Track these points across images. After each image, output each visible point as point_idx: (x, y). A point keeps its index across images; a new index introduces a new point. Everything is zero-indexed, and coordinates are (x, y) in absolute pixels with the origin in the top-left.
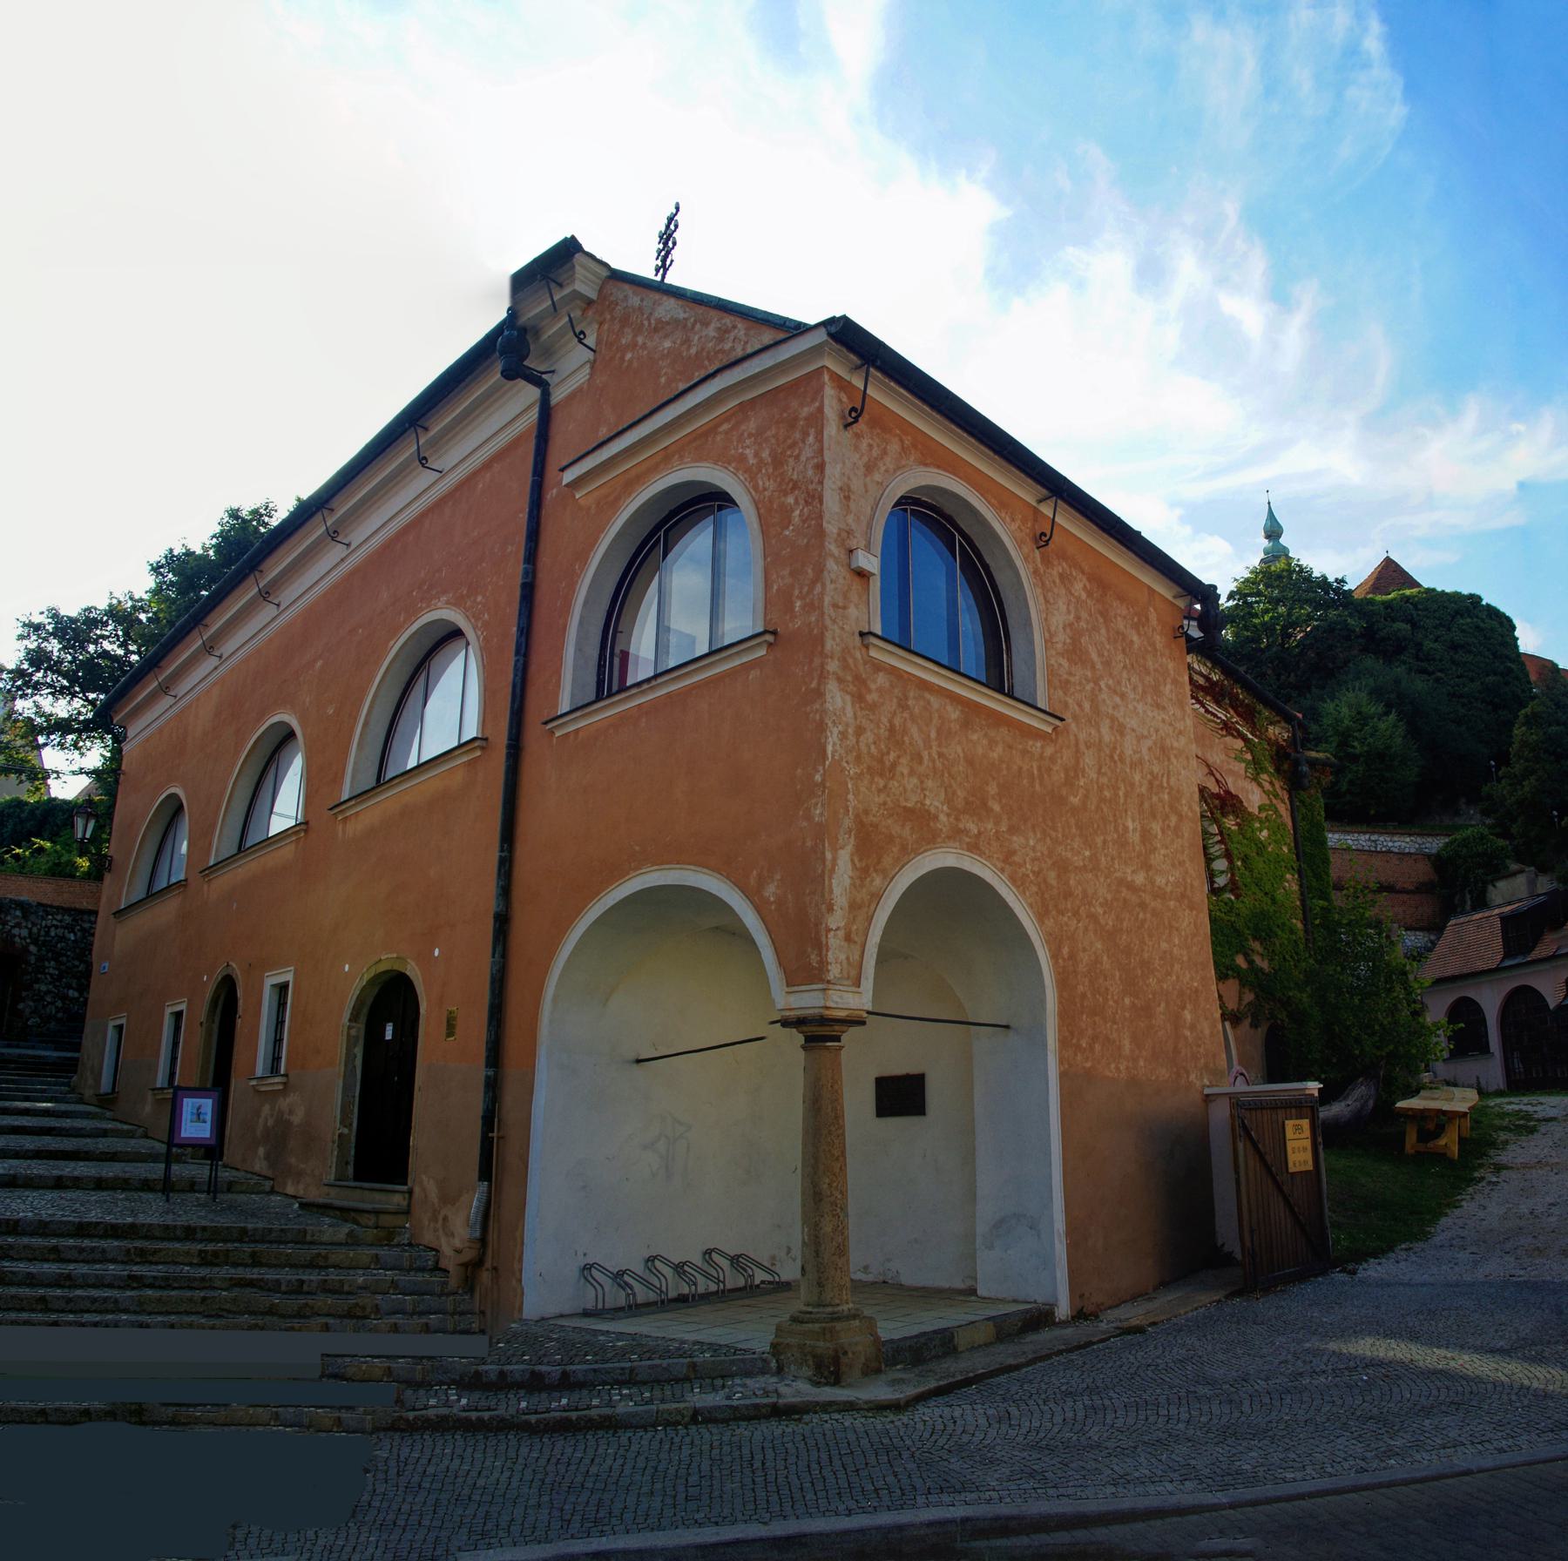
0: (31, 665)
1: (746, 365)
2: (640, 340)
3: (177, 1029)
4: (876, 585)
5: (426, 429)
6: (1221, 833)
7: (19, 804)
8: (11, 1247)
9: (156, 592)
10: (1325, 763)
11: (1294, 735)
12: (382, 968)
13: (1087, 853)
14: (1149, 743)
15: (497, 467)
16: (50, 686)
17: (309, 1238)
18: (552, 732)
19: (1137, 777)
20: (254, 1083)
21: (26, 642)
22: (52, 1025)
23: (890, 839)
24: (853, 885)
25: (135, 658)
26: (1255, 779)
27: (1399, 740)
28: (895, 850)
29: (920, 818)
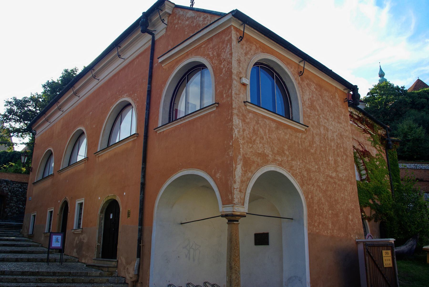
0: (8, 113)
1: (210, 27)
2: (180, 22)
3: (51, 216)
4: (248, 88)
5: (120, 47)
6: (363, 163)
7: (5, 153)
8: (2, 279)
9: (44, 93)
10: (397, 141)
11: (387, 132)
12: (109, 198)
13: (317, 167)
14: (336, 134)
15: (140, 58)
16: (14, 119)
17: (89, 275)
18: (156, 132)
19: (333, 144)
20: (73, 231)
21: (7, 107)
22: (15, 215)
23: (254, 162)
24: (242, 175)
25: (38, 111)
26: (374, 146)
27: (423, 135)
28: (255, 165)
29: (263, 156)
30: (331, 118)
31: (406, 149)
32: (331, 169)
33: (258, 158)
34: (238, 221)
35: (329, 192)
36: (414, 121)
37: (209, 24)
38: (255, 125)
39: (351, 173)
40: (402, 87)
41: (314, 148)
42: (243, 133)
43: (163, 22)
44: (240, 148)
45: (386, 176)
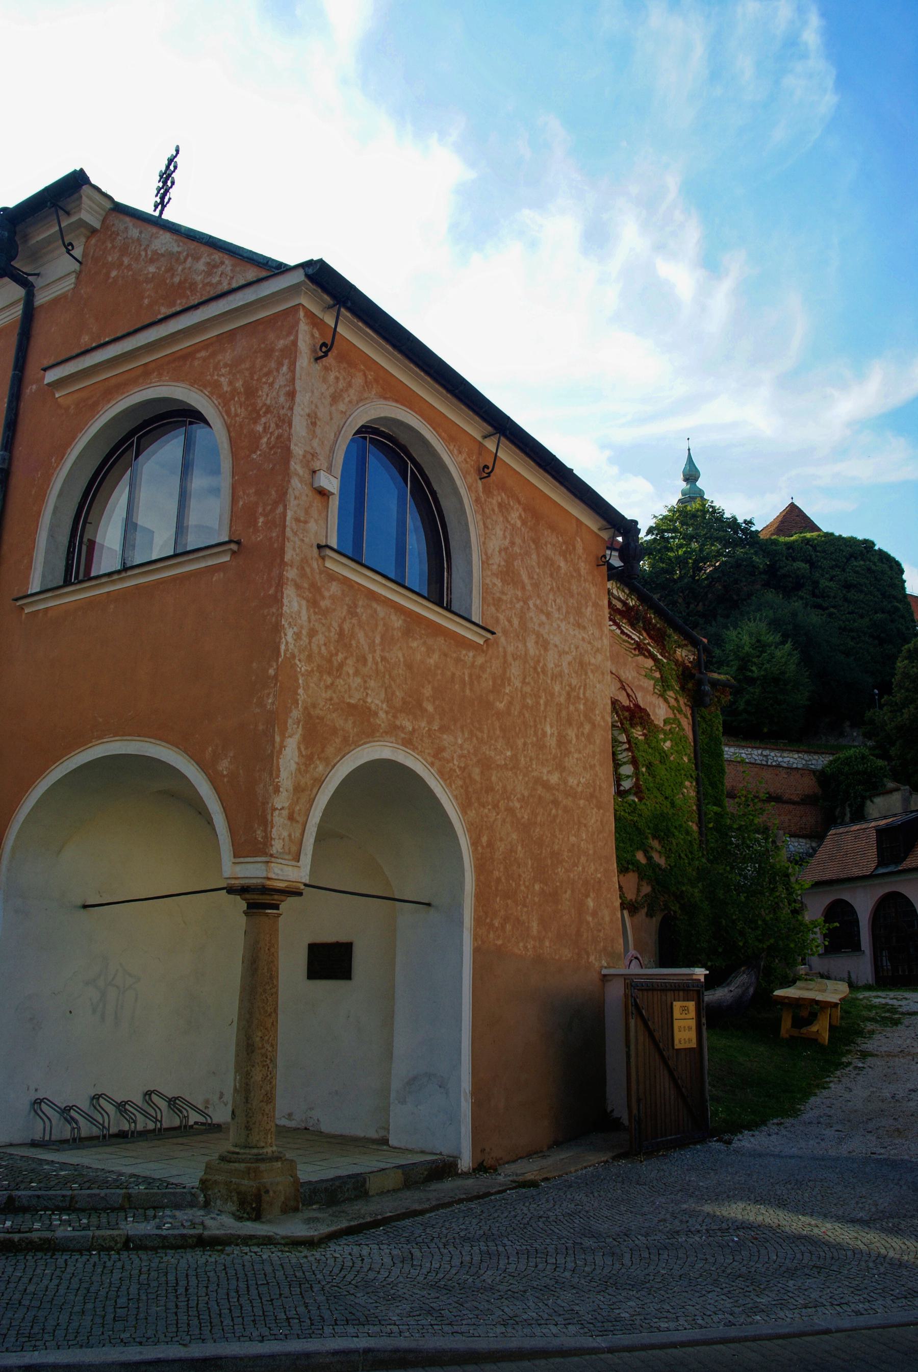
1: (231, 298)
2: (126, 261)
4: (334, 503)
6: (629, 742)
10: (725, 685)
11: (699, 657)
13: (509, 753)
14: (569, 658)
18: (21, 608)
19: (557, 688)
23: (334, 731)
26: (662, 696)
27: (793, 667)
29: (362, 714)
30: (559, 609)
31: (742, 706)
32: (547, 760)
33: (346, 720)
34: (276, 907)
35: (538, 830)
36: (769, 624)
37: (225, 287)
38: (344, 619)
39: (601, 775)
40: (745, 521)
41: (506, 697)
42: (310, 643)
43: (68, 252)
44: (298, 687)
45: (687, 783)
